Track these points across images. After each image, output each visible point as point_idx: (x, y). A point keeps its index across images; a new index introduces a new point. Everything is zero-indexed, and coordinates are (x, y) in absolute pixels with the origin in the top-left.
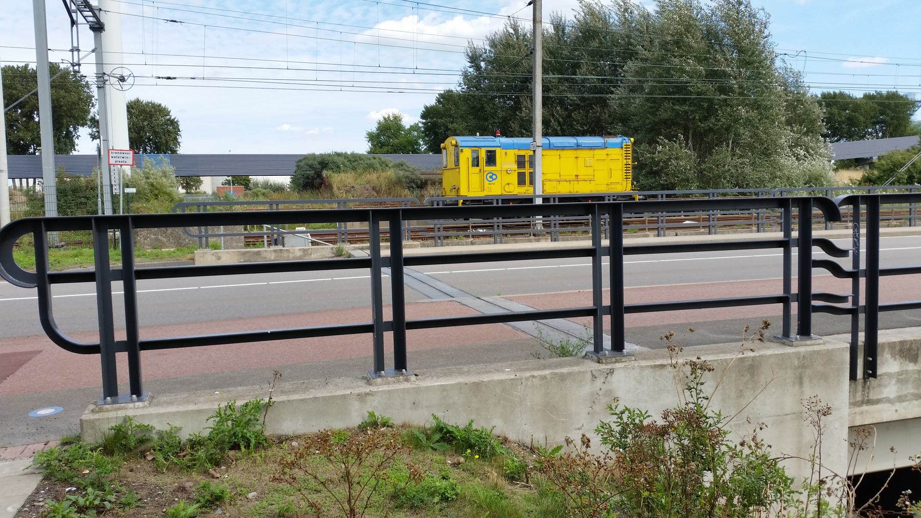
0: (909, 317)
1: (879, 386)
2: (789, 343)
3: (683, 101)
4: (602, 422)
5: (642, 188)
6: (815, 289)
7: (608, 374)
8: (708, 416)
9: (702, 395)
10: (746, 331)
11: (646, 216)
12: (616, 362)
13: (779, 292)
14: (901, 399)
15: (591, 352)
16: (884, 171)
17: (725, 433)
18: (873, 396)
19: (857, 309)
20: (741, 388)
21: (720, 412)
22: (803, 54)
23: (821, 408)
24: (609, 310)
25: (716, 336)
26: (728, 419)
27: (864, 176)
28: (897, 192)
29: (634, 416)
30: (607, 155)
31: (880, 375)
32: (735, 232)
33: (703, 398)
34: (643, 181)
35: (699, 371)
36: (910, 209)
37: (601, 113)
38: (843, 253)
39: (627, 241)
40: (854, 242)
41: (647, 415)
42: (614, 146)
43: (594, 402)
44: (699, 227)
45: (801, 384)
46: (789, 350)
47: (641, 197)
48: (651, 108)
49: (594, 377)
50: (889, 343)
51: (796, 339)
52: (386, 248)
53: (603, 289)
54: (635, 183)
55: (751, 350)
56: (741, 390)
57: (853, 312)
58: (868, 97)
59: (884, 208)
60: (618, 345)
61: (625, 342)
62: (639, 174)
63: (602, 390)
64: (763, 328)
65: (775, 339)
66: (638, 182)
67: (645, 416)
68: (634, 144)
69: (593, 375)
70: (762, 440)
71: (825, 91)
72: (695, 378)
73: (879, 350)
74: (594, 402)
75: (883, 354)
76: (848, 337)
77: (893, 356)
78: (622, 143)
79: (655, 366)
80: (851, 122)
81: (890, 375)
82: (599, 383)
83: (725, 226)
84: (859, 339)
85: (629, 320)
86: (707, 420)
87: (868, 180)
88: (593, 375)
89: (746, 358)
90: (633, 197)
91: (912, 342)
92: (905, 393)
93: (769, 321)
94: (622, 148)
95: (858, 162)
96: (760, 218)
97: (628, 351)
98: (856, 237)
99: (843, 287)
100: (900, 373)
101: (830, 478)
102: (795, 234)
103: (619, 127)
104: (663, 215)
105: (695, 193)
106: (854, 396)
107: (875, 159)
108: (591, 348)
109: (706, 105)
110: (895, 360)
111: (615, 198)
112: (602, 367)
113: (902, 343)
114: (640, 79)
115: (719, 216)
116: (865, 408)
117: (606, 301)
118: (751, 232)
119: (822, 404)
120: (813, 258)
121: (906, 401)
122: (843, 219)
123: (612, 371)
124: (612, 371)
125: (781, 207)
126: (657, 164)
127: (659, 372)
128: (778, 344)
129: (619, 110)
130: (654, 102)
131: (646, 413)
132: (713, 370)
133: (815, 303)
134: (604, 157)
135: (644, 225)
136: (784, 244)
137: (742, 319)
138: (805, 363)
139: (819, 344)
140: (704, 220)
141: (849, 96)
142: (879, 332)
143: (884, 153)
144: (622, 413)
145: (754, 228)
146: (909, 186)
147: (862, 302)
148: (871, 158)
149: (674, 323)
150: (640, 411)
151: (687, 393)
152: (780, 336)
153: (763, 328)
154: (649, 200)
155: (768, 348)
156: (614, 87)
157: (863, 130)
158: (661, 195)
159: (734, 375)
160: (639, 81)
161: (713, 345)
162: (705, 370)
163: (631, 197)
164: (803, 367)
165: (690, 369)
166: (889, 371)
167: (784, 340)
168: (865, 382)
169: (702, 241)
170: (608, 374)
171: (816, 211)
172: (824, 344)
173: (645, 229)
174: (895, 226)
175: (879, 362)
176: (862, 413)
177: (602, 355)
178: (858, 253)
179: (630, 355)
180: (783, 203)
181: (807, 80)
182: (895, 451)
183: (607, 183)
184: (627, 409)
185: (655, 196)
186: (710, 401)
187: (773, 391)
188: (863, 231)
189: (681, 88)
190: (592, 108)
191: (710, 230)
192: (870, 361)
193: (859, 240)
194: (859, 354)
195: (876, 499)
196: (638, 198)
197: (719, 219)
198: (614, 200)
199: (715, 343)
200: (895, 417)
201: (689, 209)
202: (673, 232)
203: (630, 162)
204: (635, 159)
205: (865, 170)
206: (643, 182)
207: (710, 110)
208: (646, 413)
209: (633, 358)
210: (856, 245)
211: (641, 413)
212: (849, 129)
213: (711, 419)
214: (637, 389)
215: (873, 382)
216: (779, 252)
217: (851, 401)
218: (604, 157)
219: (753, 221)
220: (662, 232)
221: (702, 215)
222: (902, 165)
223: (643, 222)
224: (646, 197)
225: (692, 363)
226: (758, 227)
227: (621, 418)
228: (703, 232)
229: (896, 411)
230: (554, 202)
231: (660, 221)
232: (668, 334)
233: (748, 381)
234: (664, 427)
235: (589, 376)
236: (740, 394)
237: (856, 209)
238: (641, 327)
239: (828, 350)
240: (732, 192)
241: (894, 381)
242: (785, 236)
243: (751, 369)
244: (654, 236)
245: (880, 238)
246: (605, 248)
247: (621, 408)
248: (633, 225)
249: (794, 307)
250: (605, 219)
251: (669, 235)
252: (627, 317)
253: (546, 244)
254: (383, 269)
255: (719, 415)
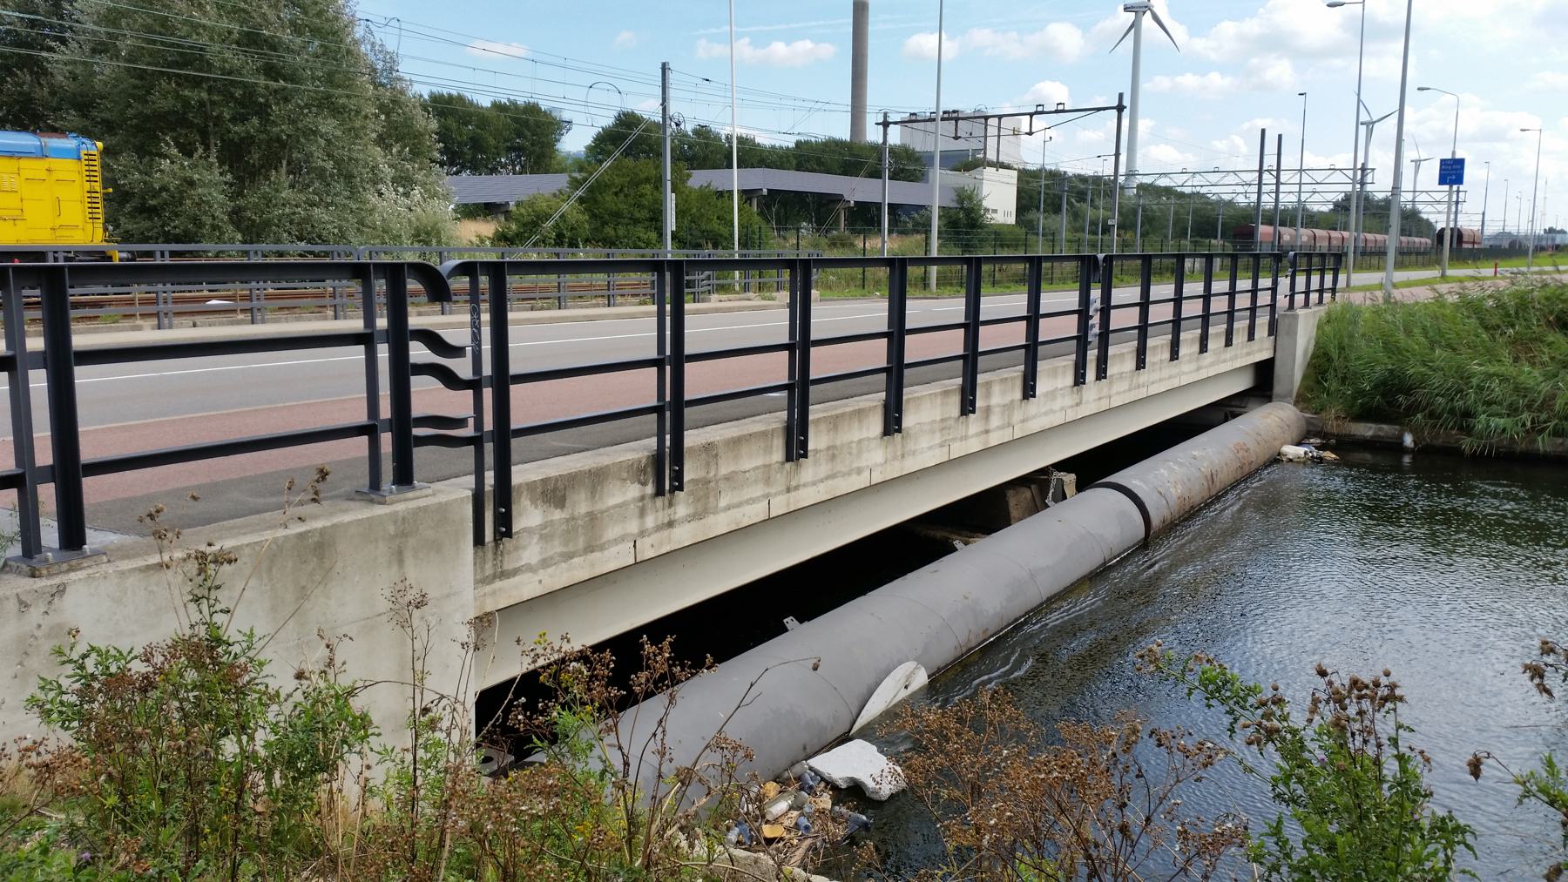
0: (554, 443)
1: (517, 548)
2: (380, 499)
3: (196, 83)
4: (42, 679)
5: (127, 238)
6: (418, 410)
7: (52, 595)
8: (231, 641)
9: (218, 607)
10: (289, 489)
11: (138, 291)
12: (71, 569)
13: (361, 418)
14: (545, 563)
15: (15, 559)
16: (524, 225)
17: (261, 664)
18: (509, 565)
19: (482, 436)
20: (303, 583)
21: (252, 630)
22: (394, 23)
23: (412, 597)
24: (49, 474)
25: (261, 501)
26: (266, 639)
27: (497, 231)
28: (534, 257)
29: (107, 660)
30: (48, 170)
31: (517, 533)
32: (298, 320)
33: (221, 611)
34: (127, 224)
35: (212, 566)
36: (559, 283)
37: (31, 86)
38: (457, 352)
39: (82, 340)
40: (473, 333)
41: (132, 655)
42: (61, 154)
43: (26, 653)
44: (234, 311)
45: (401, 562)
46: (379, 510)
47: (124, 255)
48: (135, 87)
49: (24, 605)
50: (527, 484)
51: (391, 492)
52: (36, 334)
53: (34, 435)
54: (111, 228)
55: (300, 519)
56: (304, 587)
57: (476, 442)
58: (498, 107)
59: (513, 281)
60: (73, 537)
61: (87, 531)
62: (118, 211)
63: (43, 627)
64: (318, 481)
65: (357, 496)
66: (117, 226)
67: (129, 658)
68: (106, 152)
69: (21, 602)
70: (344, 663)
71: (435, 90)
72: (205, 580)
73: (514, 495)
74: (26, 653)
75: (519, 501)
76: (471, 480)
77: (533, 502)
78: (78, 149)
79: (148, 568)
80: (476, 143)
81: (529, 531)
82: (35, 615)
83: (281, 309)
84: (486, 481)
85: (93, 489)
86: (230, 648)
87: (502, 238)
88: (21, 602)
89: (309, 532)
90: (109, 254)
91: (557, 479)
92: (550, 553)
93: (327, 468)
94: (79, 159)
95: (489, 210)
96: (338, 295)
97: (93, 547)
98: (476, 326)
99: (459, 404)
100: (544, 526)
101: (435, 703)
102: (382, 323)
103: (72, 116)
104: (165, 290)
105: (233, 249)
106: (483, 569)
107: (512, 207)
108: (16, 550)
109: (238, 93)
110: (536, 507)
111: (72, 255)
112: (39, 583)
113: (545, 481)
114: (111, 30)
115: (270, 291)
116: (498, 584)
117: (44, 455)
118: (325, 318)
119: (413, 592)
120: (412, 360)
121: (552, 565)
122: (454, 298)
123: (61, 588)
124: (61, 588)
125: (465, 275)
126: (156, 194)
127: (156, 577)
128: (362, 503)
129: (70, 86)
130: (141, 78)
131: (130, 652)
132: (236, 560)
133: (418, 431)
134: (43, 175)
135: (133, 308)
136: (365, 339)
137: (306, 467)
138: (405, 529)
139: (427, 496)
140: (243, 298)
141: (471, 103)
142: (514, 468)
143: (525, 198)
144: (84, 656)
145: (330, 313)
146: (558, 249)
147: (488, 425)
148: (507, 203)
149: (184, 485)
150: (118, 651)
151: (192, 607)
152: (366, 489)
153: (318, 481)
154: (139, 262)
155: (346, 511)
156: (56, 39)
157: (494, 159)
158: (162, 256)
159: (290, 564)
160: (109, 33)
161: (253, 517)
162: (222, 563)
163: (104, 255)
164: (404, 535)
165: (197, 566)
166: (530, 525)
167: (373, 496)
168: (497, 546)
169: (240, 336)
170: (52, 595)
171: (412, 285)
172: (434, 495)
173: (134, 315)
174: (542, 309)
175: (514, 513)
176: (494, 593)
177: (40, 562)
178: (480, 351)
179: (97, 553)
180: (360, 272)
181: (405, 69)
182: (521, 643)
183: (50, 225)
184: (93, 649)
185: (150, 254)
186: (232, 614)
187: (356, 579)
188: (486, 317)
189: (192, 58)
190: (12, 74)
191: (253, 316)
192: (502, 513)
193: (479, 330)
194: (486, 504)
195: (497, 719)
196: (118, 256)
197: (269, 297)
198: (66, 259)
199: (258, 512)
200: (538, 591)
201: (192, 280)
202: (188, 320)
203: (98, 187)
204: (106, 182)
205: (499, 222)
206: (130, 227)
207: (250, 105)
208: (130, 652)
209: (105, 559)
210: (476, 338)
211: (121, 654)
212: (474, 157)
213: (237, 645)
214: (115, 613)
215: (507, 545)
216: (357, 353)
217: (478, 577)
218: (43, 175)
219: (327, 301)
220: (166, 321)
221: (238, 288)
222: (547, 217)
223: (131, 302)
224: (135, 255)
225: (199, 555)
226: (335, 312)
227: (82, 667)
228: (242, 320)
229: (540, 582)
230: (56, 259)
231: (161, 301)
232: (153, 510)
233: (314, 569)
234: (146, 677)
235: (12, 605)
236: (303, 594)
237: (474, 283)
238: (126, 500)
239: (440, 503)
240: (294, 250)
241: (536, 538)
242: (366, 327)
243: (320, 548)
244: (153, 329)
245: (510, 328)
246: (33, 353)
247: (81, 648)
248: (112, 308)
249: (386, 439)
250: (157, 293)
251: (181, 326)
252: (88, 483)
253: (148, 335)
254: (32, 374)
255: (251, 635)
